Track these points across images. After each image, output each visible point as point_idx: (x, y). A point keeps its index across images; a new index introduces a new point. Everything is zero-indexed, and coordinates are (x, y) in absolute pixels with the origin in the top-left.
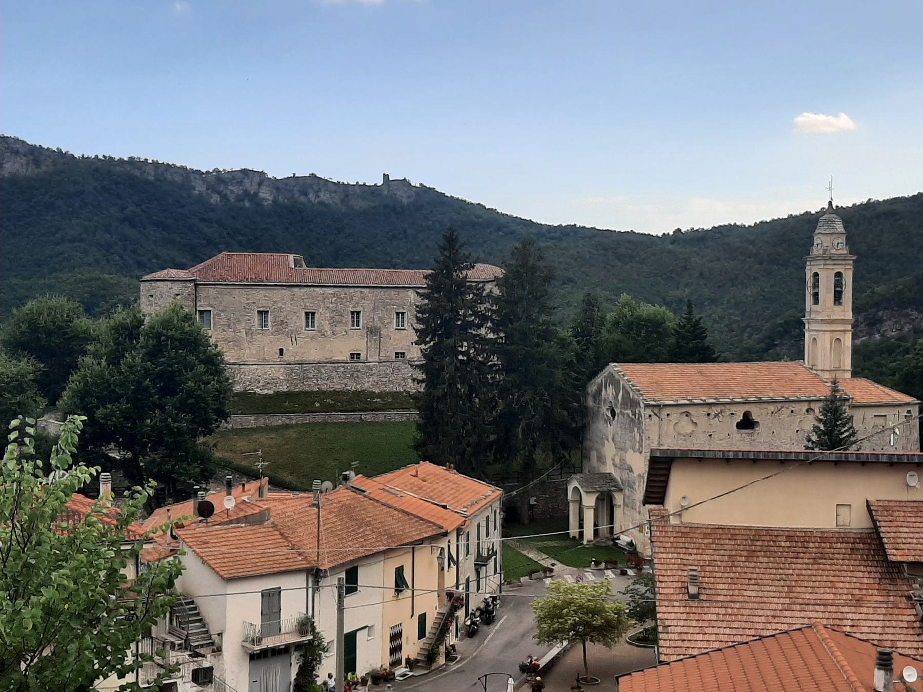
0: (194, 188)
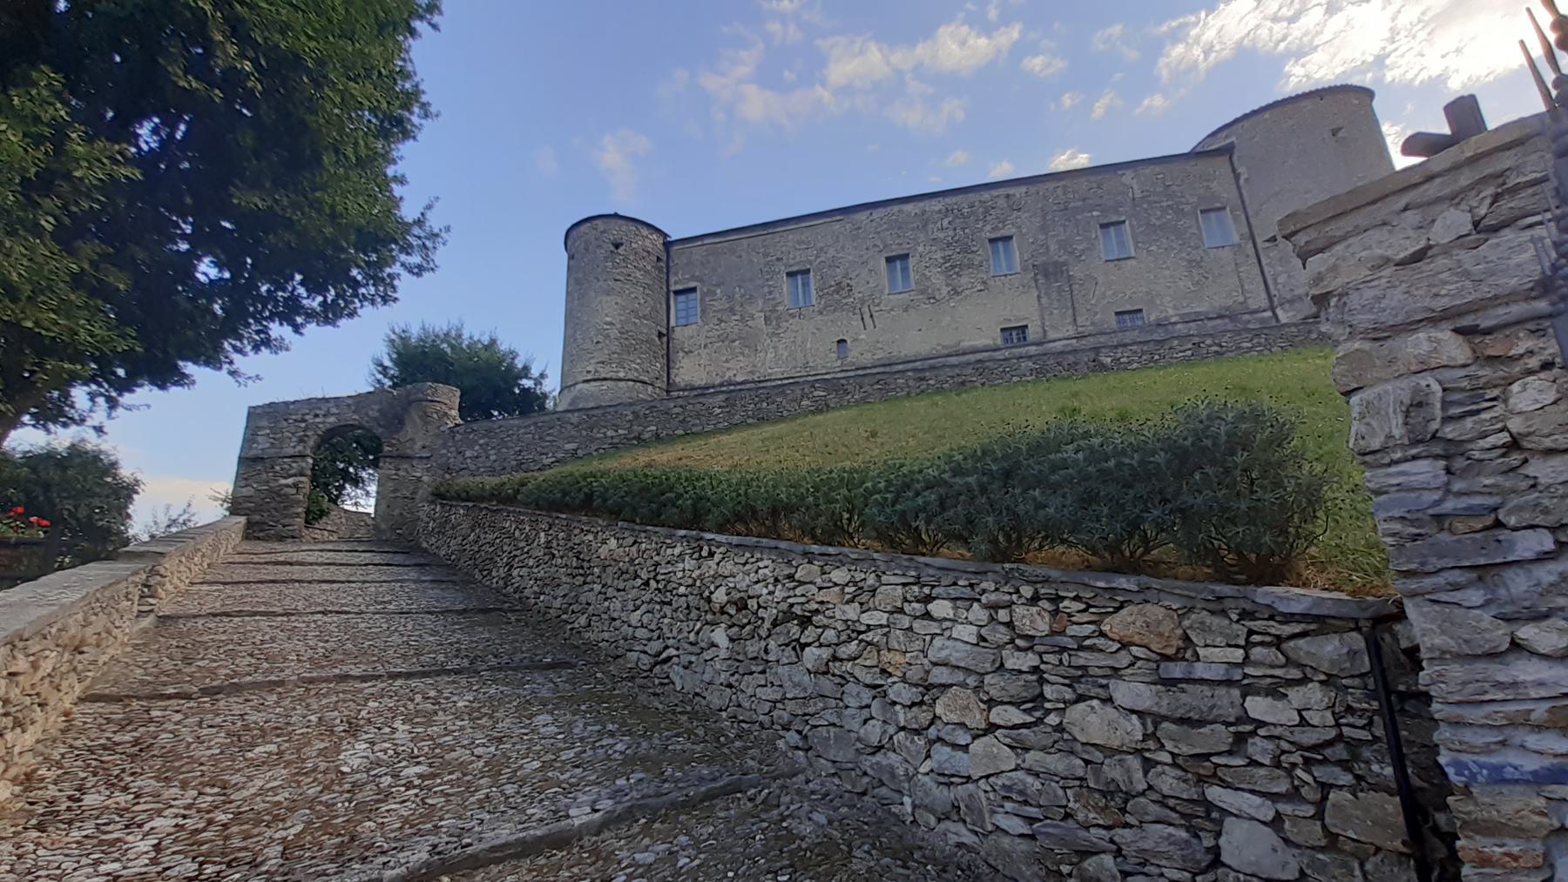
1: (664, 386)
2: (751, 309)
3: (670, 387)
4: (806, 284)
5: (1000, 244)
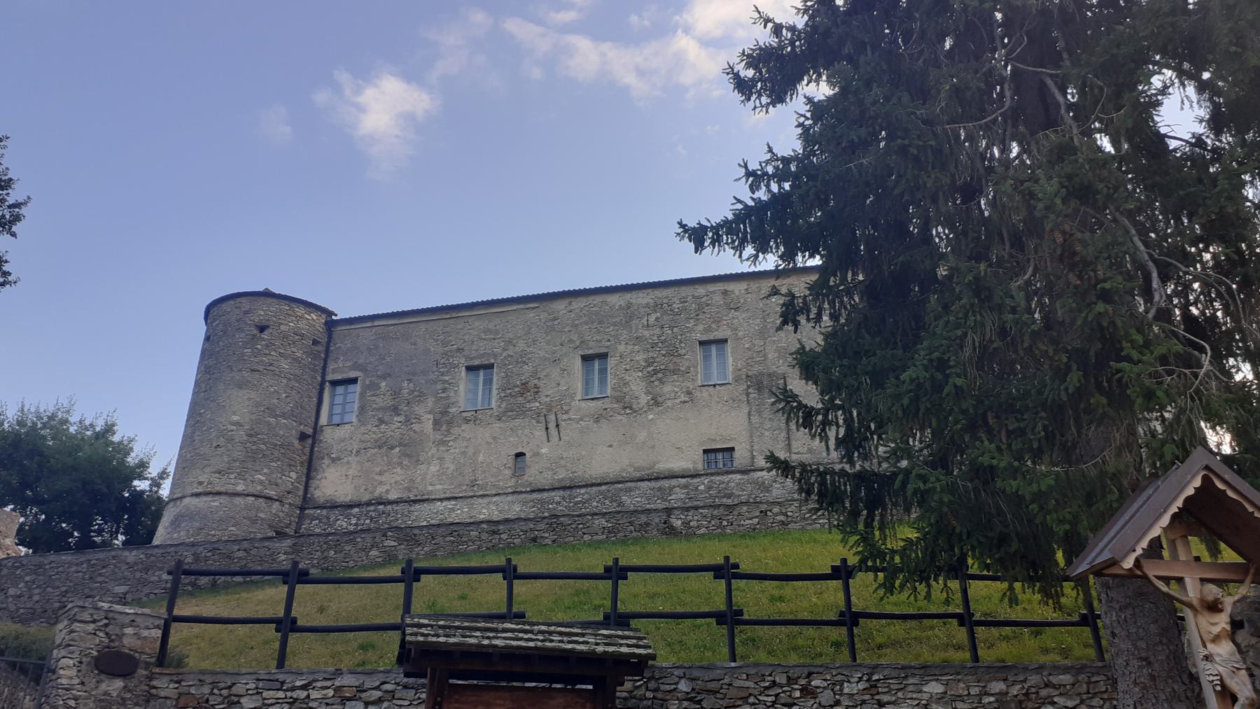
0: (408, 119)
1: (298, 501)
2: (419, 409)
3: (307, 503)
4: (488, 382)
5: (714, 348)
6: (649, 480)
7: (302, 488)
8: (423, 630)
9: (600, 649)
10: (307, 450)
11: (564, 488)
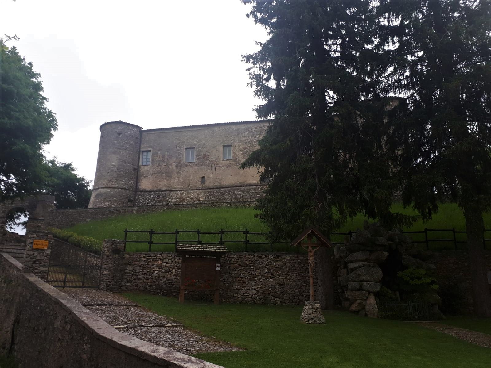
4: (193, 153)
6: (243, 186)
7: (135, 185)
8: (181, 247)
9: (217, 250)
10: (136, 174)
11: (217, 188)
